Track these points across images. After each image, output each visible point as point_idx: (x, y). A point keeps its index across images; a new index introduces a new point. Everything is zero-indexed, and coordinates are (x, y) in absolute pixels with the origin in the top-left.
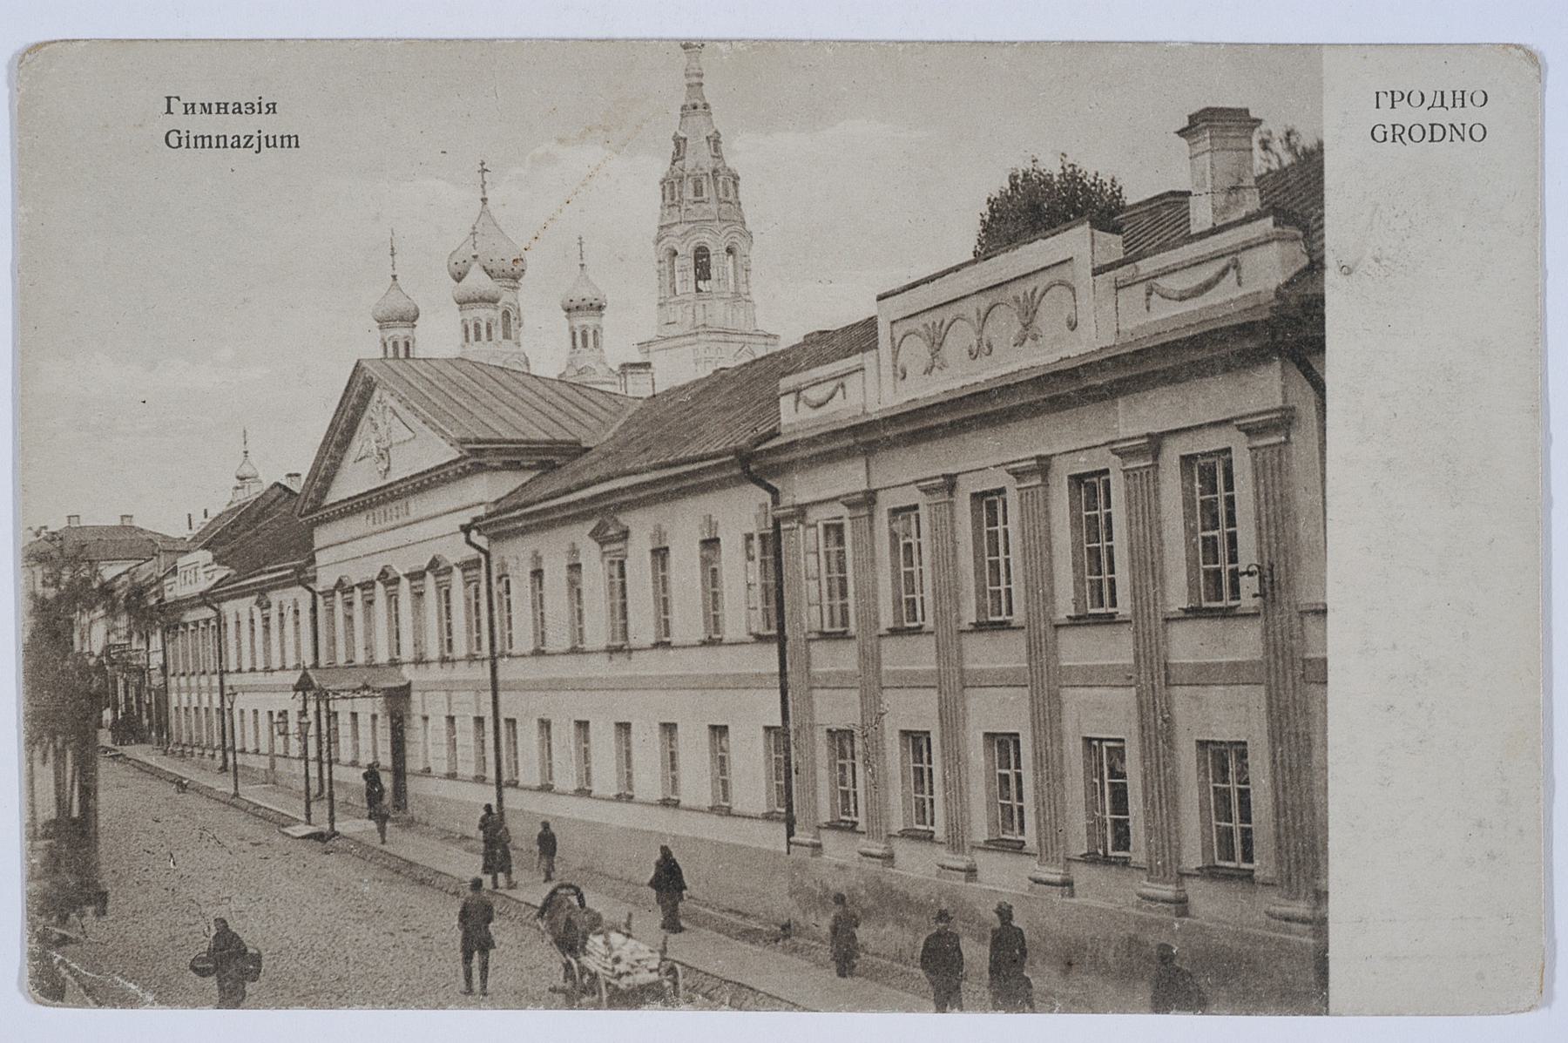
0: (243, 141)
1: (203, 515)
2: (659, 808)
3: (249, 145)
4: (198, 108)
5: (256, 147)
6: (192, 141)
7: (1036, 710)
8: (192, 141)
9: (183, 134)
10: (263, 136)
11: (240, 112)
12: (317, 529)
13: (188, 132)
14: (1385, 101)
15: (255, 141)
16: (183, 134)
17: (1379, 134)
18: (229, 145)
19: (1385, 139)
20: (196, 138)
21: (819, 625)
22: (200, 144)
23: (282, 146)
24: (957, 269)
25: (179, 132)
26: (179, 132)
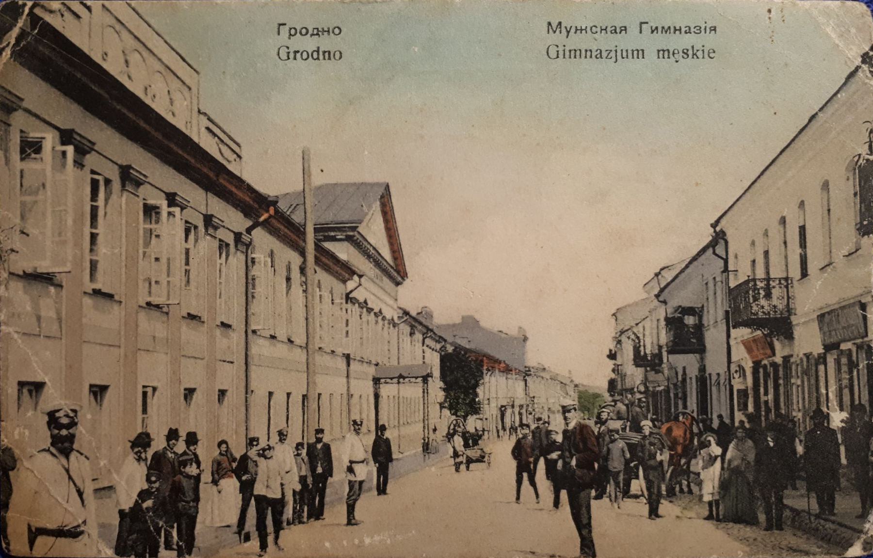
0: (604, 54)
1: (350, 321)
2: (623, 460)
3: (609, 57)
4: (660, 29)
5: (614, 59)
6: (567, 53)
7: (845, 382)
8: (567, 53)
9: (561, 49)
10: (567, 49)
11: (616, 32)
12: (457, 322)
13: (564, 46)
14: (284, 30)
15: (613, 54)
16: (561, 49)
17: (553, 53)
18: (593, 56)
19: (558, 57)
20: (570, 51)
21: (401, 388)
22: (572, 56)
23: (664, 58)
24: (793, 140)
25: (288, 48)
26: (288, 48)
